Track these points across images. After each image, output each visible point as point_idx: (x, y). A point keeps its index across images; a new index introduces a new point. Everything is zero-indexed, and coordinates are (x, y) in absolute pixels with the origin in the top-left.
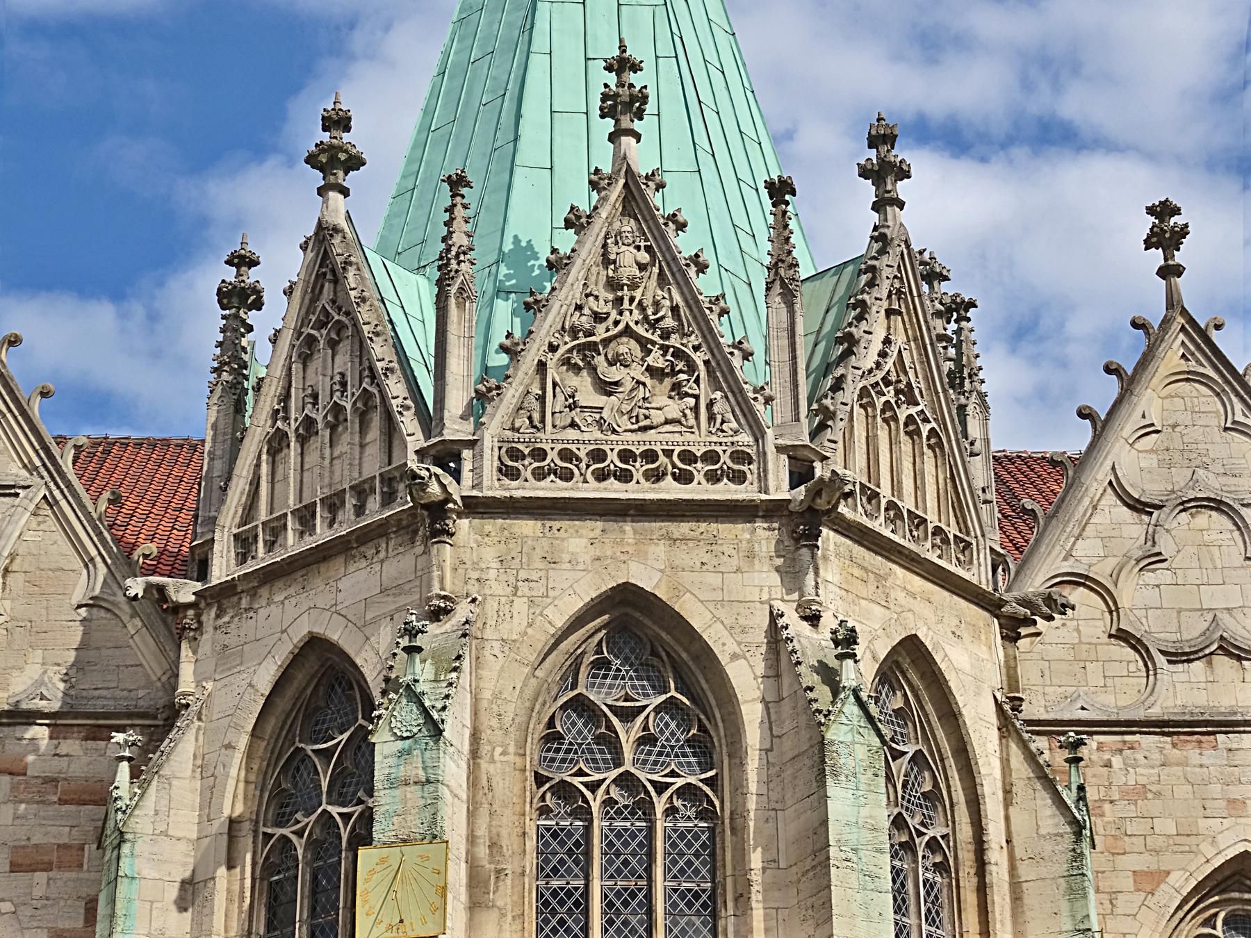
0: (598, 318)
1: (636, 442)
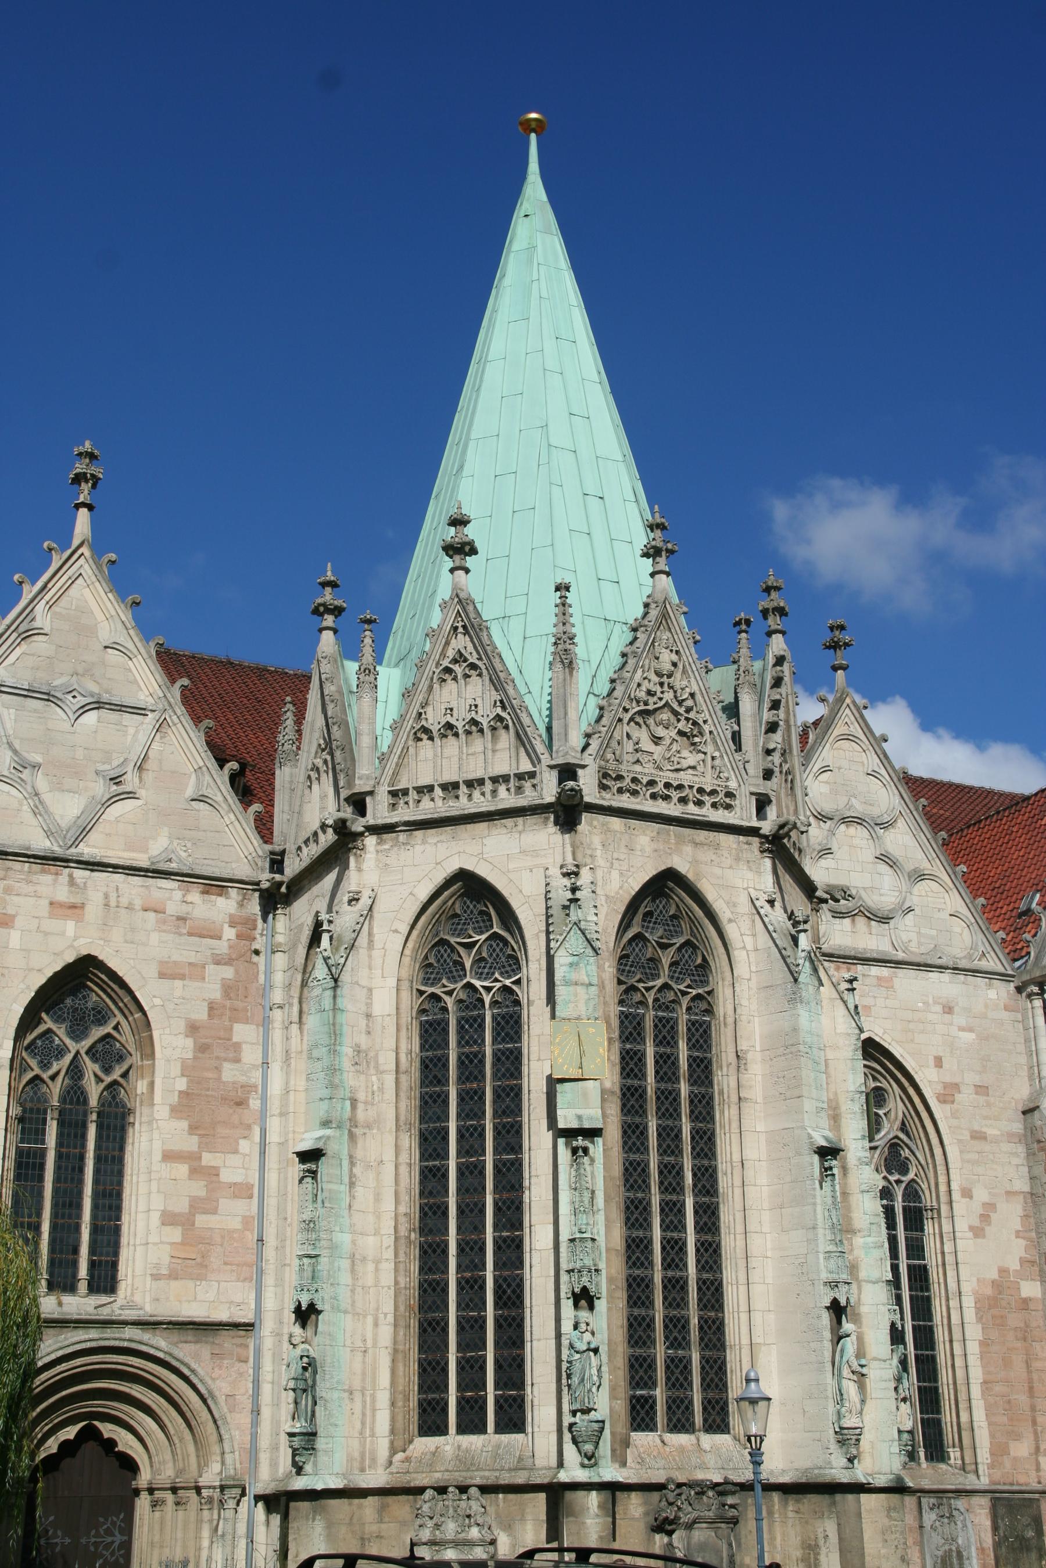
0: (649, 693)
1: (674, 779)
